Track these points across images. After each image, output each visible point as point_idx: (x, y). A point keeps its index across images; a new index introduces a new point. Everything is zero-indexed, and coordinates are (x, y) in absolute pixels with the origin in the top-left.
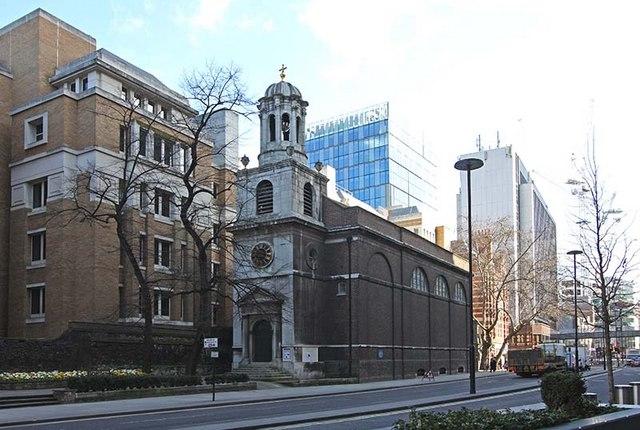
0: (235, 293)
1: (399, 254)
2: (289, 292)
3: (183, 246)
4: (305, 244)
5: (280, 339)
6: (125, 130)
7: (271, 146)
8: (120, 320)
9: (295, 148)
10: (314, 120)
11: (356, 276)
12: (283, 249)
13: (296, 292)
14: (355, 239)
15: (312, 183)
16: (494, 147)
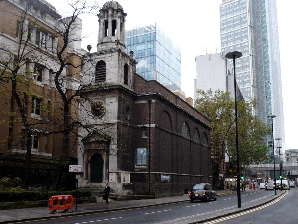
0: (83, 133)
1: (176, 113)
2: (113, 133)
3: (49, 102)
4: (124, 103)
5: (108, 167)
6: (20, 23)
7: (105, 40)
8: (9, 151)
10: (130, 25)
12: (111, 105)
13: (119, 134)
15: (128, 64)
16: (214, 52)
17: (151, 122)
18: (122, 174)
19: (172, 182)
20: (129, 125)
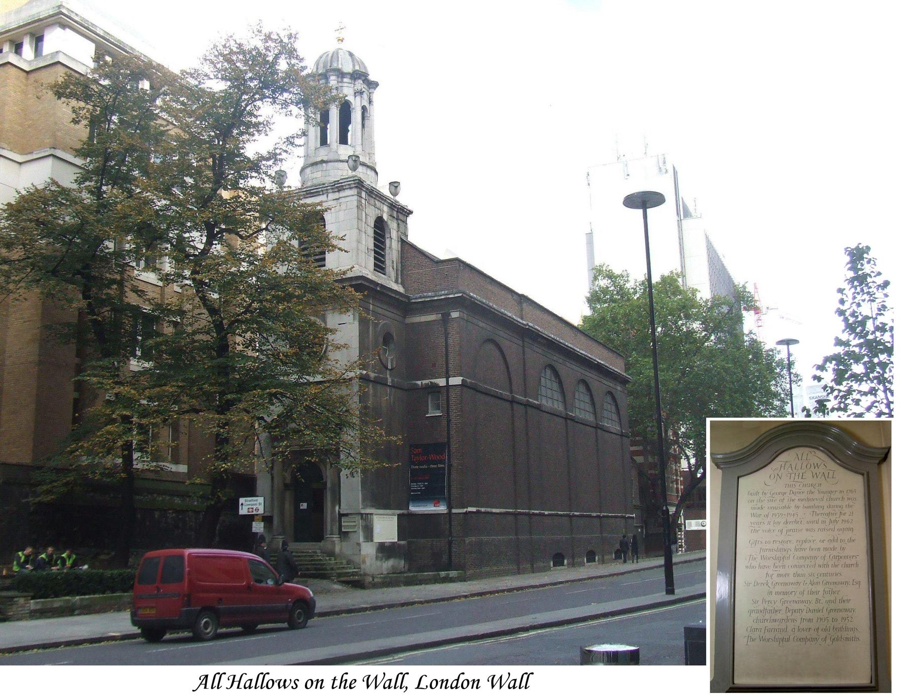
1: (520, 343)
7: (323, 154)
9: (362, 159)
11: (456, 381)
14: (455, 315)
15: (385, 217)
17: (451, 373)
18: (375, 517)
19: (531, 534)
20: (393, 381)
